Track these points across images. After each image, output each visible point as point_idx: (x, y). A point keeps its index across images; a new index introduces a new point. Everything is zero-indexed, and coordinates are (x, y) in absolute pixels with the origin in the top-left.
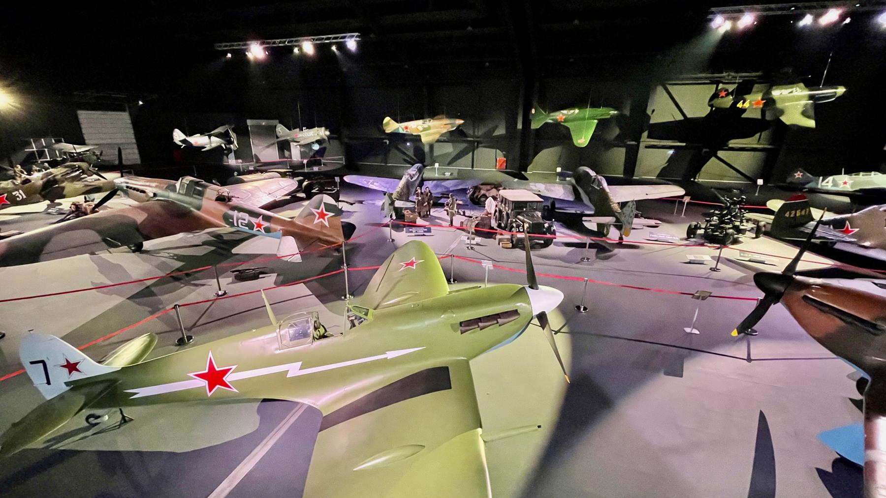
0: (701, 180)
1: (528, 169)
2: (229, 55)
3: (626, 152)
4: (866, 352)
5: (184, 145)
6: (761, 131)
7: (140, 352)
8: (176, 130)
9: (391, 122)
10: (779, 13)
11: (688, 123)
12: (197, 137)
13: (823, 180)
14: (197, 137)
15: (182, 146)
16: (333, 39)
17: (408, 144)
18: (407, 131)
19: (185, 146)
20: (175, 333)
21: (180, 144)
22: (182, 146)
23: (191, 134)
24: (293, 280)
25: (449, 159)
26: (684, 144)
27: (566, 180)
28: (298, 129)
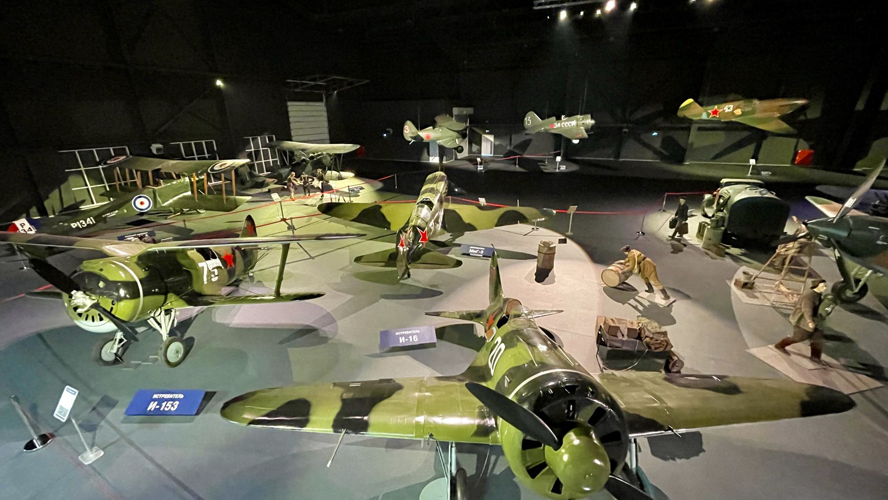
4: (632, 323)
5: (413, 141)
7: (309, 294)
8: (409, 122)
10: (548, 7)
12: (429, 130)
14: (429, 130)
15: (410, 142)
19: (414, 142)
21: (410, 139)
22: (410, 142)
23: (422, 127)
28: (554, 118)
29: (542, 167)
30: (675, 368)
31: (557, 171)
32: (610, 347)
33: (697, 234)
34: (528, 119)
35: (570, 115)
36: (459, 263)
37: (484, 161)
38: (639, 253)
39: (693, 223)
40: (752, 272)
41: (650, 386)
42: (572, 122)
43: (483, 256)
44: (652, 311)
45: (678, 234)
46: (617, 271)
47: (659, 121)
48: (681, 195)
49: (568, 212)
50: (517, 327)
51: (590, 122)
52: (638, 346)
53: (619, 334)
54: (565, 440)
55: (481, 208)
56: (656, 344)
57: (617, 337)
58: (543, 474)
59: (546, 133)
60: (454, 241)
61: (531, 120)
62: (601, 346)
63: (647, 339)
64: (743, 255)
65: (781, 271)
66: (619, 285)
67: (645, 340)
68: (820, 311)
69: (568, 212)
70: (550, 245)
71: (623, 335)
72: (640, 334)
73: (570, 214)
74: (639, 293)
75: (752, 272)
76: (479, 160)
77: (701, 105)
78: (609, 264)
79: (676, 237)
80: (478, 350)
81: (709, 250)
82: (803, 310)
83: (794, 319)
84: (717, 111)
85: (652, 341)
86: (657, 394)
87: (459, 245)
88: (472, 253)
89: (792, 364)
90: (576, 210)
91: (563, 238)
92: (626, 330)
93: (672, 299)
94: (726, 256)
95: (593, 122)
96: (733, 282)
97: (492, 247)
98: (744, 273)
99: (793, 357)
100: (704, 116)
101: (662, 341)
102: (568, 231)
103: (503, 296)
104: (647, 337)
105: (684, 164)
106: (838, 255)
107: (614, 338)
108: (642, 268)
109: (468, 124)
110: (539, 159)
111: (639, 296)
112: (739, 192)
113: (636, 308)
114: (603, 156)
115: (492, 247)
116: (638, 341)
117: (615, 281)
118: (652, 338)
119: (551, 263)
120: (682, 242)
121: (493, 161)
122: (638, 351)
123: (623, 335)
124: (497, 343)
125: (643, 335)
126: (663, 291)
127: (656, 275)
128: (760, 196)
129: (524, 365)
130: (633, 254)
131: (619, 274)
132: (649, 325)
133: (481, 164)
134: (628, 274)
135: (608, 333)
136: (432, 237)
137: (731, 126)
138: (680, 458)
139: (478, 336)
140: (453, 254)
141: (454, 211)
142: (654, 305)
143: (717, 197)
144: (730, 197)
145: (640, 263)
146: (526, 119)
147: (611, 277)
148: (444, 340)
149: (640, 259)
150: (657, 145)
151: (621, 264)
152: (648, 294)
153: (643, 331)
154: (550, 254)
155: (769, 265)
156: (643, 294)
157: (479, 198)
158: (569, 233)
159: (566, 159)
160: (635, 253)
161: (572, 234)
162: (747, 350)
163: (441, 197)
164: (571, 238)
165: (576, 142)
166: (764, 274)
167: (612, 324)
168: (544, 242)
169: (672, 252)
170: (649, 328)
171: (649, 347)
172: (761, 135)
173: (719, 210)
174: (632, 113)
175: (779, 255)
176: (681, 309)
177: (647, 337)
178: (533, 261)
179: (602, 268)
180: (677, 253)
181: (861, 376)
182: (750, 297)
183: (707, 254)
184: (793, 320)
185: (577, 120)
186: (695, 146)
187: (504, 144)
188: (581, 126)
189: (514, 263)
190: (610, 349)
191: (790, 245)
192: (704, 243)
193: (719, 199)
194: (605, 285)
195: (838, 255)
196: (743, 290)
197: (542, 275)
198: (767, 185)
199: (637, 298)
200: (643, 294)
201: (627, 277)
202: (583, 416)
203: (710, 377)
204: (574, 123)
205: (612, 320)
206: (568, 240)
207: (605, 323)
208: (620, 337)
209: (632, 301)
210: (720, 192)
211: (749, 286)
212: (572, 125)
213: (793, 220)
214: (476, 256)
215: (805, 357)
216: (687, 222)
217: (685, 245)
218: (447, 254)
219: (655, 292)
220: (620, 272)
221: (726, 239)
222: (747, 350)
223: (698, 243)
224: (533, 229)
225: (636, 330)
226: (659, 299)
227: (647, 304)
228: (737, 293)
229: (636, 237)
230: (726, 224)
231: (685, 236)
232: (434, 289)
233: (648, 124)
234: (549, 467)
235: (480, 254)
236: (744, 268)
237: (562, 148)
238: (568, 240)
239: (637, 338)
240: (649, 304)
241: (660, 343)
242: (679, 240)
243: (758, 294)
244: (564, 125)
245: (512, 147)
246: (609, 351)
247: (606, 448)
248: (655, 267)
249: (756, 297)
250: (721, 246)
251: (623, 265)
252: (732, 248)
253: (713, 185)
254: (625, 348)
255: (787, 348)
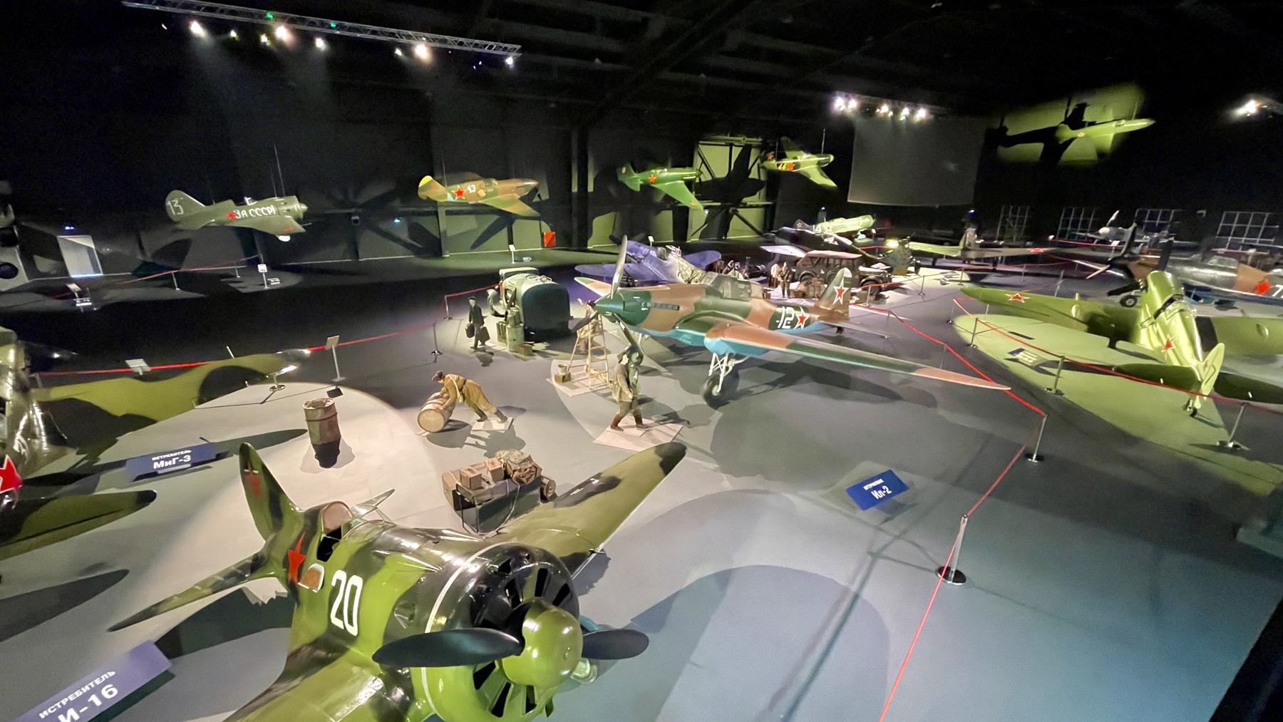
0: (732, 238)
1: (588, 243)
2: (233, 34)
3: (673, 214)
6: (760, 189)
9: (432, 184)
11: (715, 181)
13: (815, 227)
16: (217, 8)
17: (397, 221)
18: (460, 199)
20: (1170, 307)
24: (391, 548)
25: (473, 241)
26: (719, 204)
27: (523, 261)
29: (233, 285)
30: (550, 491)
31: (266, 287)
32: (479, 505)
33: (498, 338)
34: (173, 204)
35: (259, 196)
36: (148, 497)
37: (87, 287)
38: (456, 376)
39: (491, 324)
40: (566, 363)
41: (546, 521)
42: (267, 208)
43: (194, 464)
44: (495, 443)
45: (479, 343)
46: (437, 409)
47: (396, 204)
48: (472, 294)
49: (327, 347)
50: (366, 539)
51: (299, 207)
52: (510, 487)
53: (484, 484)
54: (524, 634)
55: (145, 378)
56: (527, 473)
57: (482, 488)
58: (510, 700)
59: (221, 228)
60: (97, 460)
61: (179, 204)
62: (466, 511)
63: (516, 473)
64: (548, 348)
65: (587, 354)
66: (445, 425)
67: (514, 476)
68: (631, 381)
69: (327, 347)
70: (325, 404)
71: (488, 482)
72: (506, 472)
73: (332, 349)
74: (472, 427)
75: (566, 363)
76: (73, 287)
77: (440, 182)
78: (422, 404)
79: (478, 347)
80: (936, 407)
81: (517, 352)
82: (620, 385)
83: (616, 395)
84: (462, 192)
85: (521, 474)
86: (562, 525)
87: (120, 464)
88: (161, 468)
89: (629, 437)
90: (339, 342)
91: (334, 388)
92: (489, 473)
93: (510, 419)
94: (535, 353)
95: (304, 207)
96: (553, 379)
97: (205, 442)
98: (560, 366)
99: (625, 430)
100: (450, 198)
101: (531, 468)
102: (336, 376)
103: (297, 509)
104: (514, 471)
105: (444, 258)
106: (623, 327)
107: (480, 491)
108: (466, 394)
109: (12, 216)
110: (221, 273)
111: (474, 431)
112: (522, 282)
113: (477, 445)
114: (333, 257)
115: (205, 442)
116: (507, 481)
117: (437, 422)
118: (520, 471)
119: (336, 430)
120: (487, 351)
121: (109, 286)
122: (510, 493)
123: (488, 482)
124: (339, 582)
125: (510, 471)
126: (498, 413)
127: (484, 397)
128: (542, 283)
129: (419, 580)
130: (449, 381)
131: (441, 412)
132: (510, 456)
133: (81, 295)
134: (450, 408)
135: (471, 489)
136: (29, 469)
137: (479, 210)
138: (596, 581)
139: (263, 603)
140: (108, 486)
141: (70, 402)
142: (495, 434)
143: (503, 293)
144: (516, 290)
145: (462, 388)
146: (169, 203)
147: (432, 419)
148: (186, 654)
149: (461, 383)
150: (404, 235)
151: (437, 398)
152: (482, 423)
153: (508, 466)
154: (328, 418)
155: (575, 353)
156: (478, 426)
157: (128, 362)
158: (339, 379)
159: (274, 267)
160: (452, 377)
161: (343, 378)
162: (594, 442)
163: (17, 379)
164: (347, 384)
165: (286, 239)
166: (575, 363)
167: (472, 475)
168: (313, 402)
169: (483, 365)
170: (513, 460)
171: (521, 482)
172: (506, 220)
173: (510, 306)
174: (356, 194)
175: (580, 339)
176: (523, 426)
177: (514, 471)
178: (299, 439)
179: (414, 413)
180: (488, 365)
181: (667, 425)
182: (573, 389)
183: (516, 356)
184: (616, 397)
185: (277, 205)
186: (450, 234)
187: (127, 252)
188: (286, 214)
189: (777, 359)
190: (479, 507)
191: (586, 327)
192: (510, 347)
193: (506, 293)
194: (427, 433)
195: (623, 327)
196: (565, 383)
197: (328, 453)
198: (542, 271)
199: (472, 433)
200: (478, 426)
201: (451, 412)
202: (527, 595)
203: (588, 482)
204: (271, 209)
205: (469, 470)
206: (342, 389)
207: (461, 478)
208: (487, 487)
209: (469, 440)
210: (503, 285)
211: (566, 378)
212: (270, 213)
213: (579, 302)
214: (166, 473)
215: (633, 427)
216: (484, 325)
217: (492, 354)
218: (93, 491)
219: (489, 418)
220: (442, 409)
221: (528, 337)
222: (594, 442)
223: (504, 348)
224: (273, 388)
225: (501, 468)
226: (497, 425)
227: (486, 435)
228: (561, 388)
229: (434, 359)
230: (522, 320)
231: (487, 343)
232: (99, 573)
233: (381, 207)
234: (514, 684)
235: (183, 463)
236: (555, 363)
237: (259, 250)
238: (342, 389)
239: (505, 478)
240: (489, 434)
241: (530, 471)
242: (483, 350)
243: (576, 384)
244: (253, 213)
245: (149, 254)
246: (481, 511)
247: (563, 607)
248: (480, 388)
249: (577, 387)
250: (527, 345)
251: (440, 399)
252: (535, 344)
253: (493, 278)
254: (496, 497)
255: (619, 425)
